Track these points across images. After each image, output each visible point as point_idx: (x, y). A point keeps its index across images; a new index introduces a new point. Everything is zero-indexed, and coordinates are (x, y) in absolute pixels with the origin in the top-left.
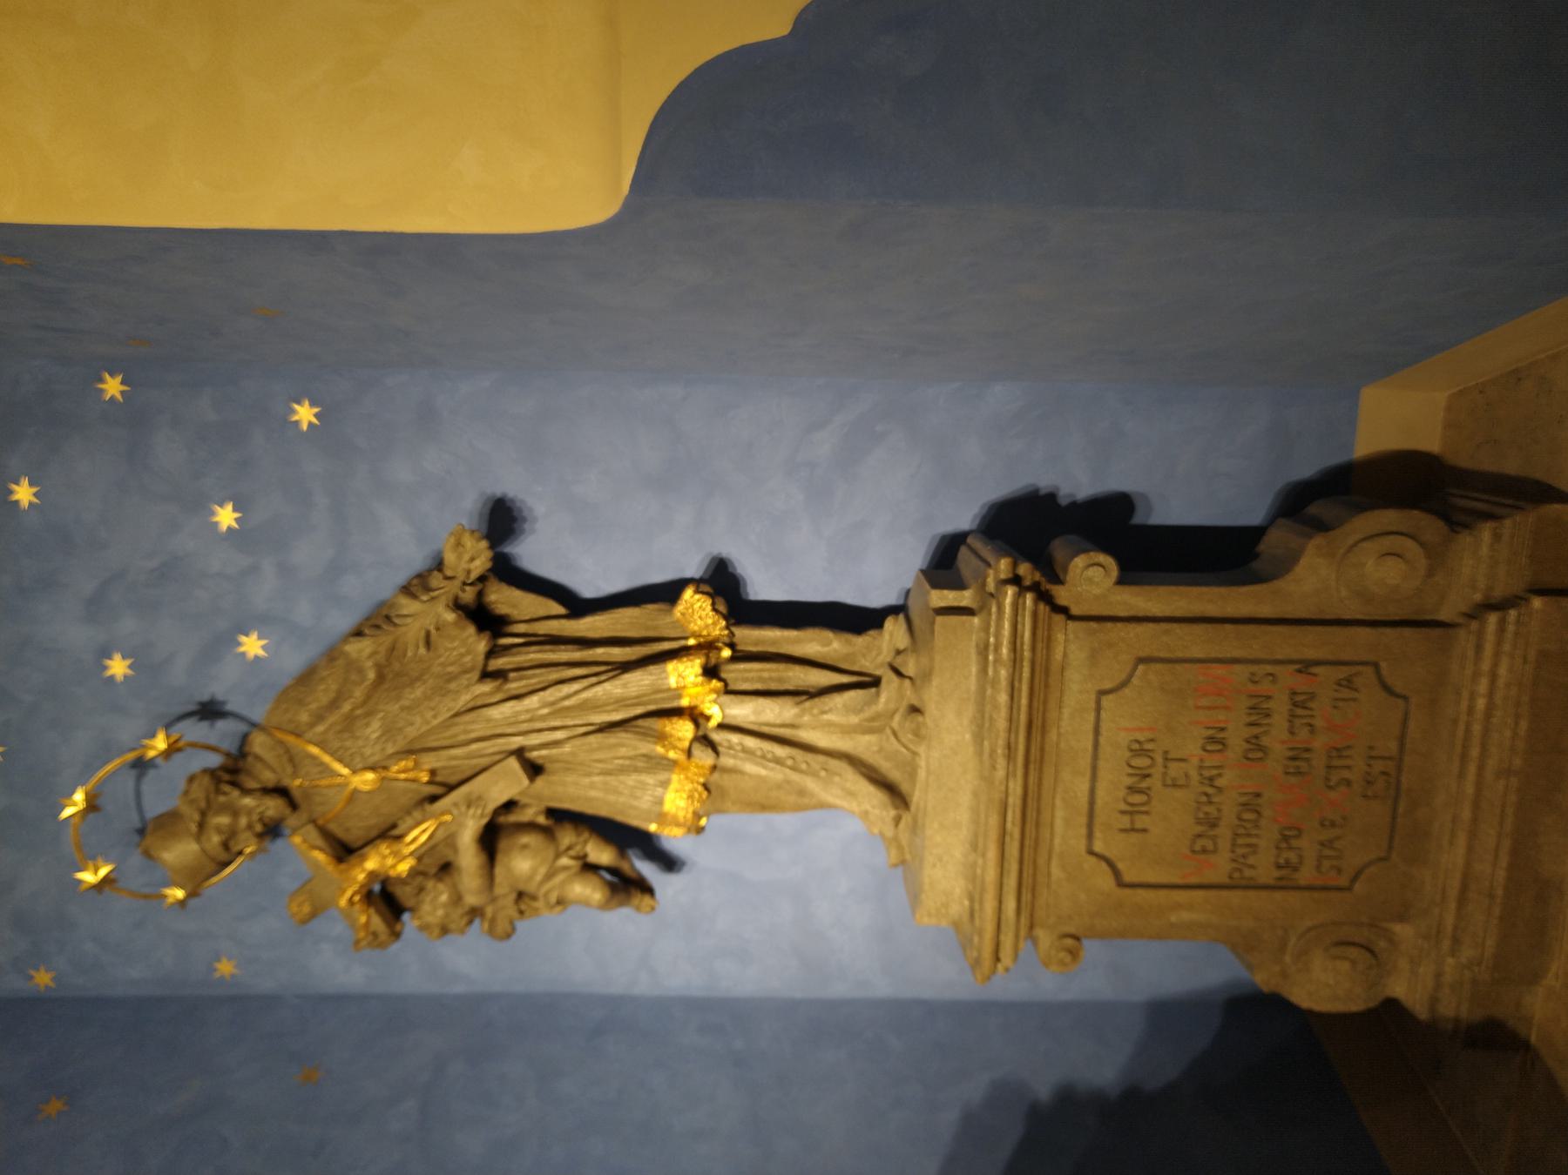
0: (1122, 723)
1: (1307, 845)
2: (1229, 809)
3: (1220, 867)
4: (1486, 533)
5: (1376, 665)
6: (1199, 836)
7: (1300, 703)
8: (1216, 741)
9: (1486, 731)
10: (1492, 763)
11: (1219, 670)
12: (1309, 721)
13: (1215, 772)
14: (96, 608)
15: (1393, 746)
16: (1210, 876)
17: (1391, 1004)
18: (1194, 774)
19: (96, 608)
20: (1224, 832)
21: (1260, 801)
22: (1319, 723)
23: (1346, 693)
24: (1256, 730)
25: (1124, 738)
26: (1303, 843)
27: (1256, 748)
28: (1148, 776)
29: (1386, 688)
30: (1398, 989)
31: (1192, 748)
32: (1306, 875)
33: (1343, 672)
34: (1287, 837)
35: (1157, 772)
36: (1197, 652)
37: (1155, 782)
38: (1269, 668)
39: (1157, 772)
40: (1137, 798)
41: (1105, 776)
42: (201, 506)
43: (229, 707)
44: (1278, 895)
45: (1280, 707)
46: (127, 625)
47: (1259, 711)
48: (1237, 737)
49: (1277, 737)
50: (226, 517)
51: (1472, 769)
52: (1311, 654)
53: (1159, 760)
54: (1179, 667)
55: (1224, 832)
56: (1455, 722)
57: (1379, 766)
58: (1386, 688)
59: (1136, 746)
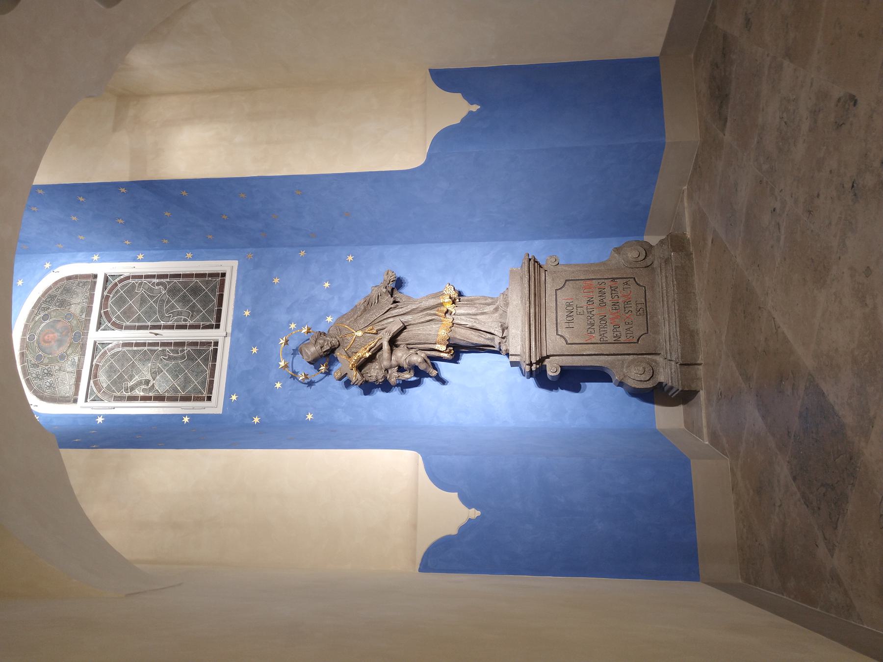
0: (564, 297)
1: (622, 329)
2: (596, 319)
3: (596, 338)
4: (515, 297)
5: (634, 279)
6: (589, 328)
7: (613, 289)
8: (590, 301)
9: (667, 292)
10: (670, 300)
11: (589, 282)
12: (617, 294)
13: (591, 310)
14: (289, 310)
15: (643, 300)
16: (594, 341)
17: (660, 383)
18: (585, 311)
19: (289, 310)
20: (596, 327)
21: (606, 318)
22: (619, 295)
23: (626, 286)
24: (602, 298)
25: (564, 302)
26: (621, 328)
27: (602, 303)
28: (572, 312)
29: (638, 284)
30: (662, 378)
31: (584, 304)
32: (623, 339)
33: (625, 280)
34: (616, 327)
35: (575, 310)
36: (378, 343)
37: (574, 314)
38: (603, 281)
39: (575, 310)
40: (570, 318)
41: (559, 314)
42: (320, 282)
43: (327, 377)
44: (615, 345)
45: (608, 290)
46: (297, 315)
47: (602, 293)
48: (597, 301)
49: (608, 298)
50: (327, 285)
51: (665, 303)
52: (614, 276)
53: (575, 308)
54: (577, 282)
55: (596, 327)
56: (659, 292)
57: (640, 306)
58: (638, 284)
59: (567, 304)
